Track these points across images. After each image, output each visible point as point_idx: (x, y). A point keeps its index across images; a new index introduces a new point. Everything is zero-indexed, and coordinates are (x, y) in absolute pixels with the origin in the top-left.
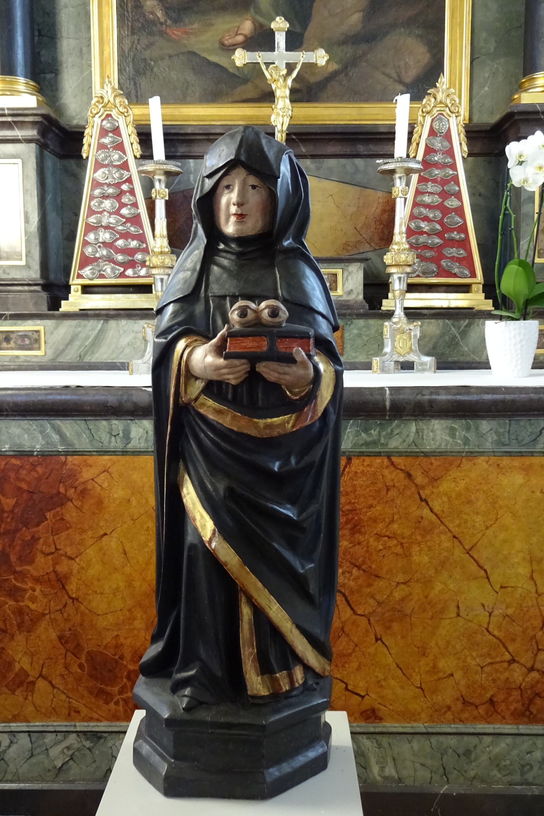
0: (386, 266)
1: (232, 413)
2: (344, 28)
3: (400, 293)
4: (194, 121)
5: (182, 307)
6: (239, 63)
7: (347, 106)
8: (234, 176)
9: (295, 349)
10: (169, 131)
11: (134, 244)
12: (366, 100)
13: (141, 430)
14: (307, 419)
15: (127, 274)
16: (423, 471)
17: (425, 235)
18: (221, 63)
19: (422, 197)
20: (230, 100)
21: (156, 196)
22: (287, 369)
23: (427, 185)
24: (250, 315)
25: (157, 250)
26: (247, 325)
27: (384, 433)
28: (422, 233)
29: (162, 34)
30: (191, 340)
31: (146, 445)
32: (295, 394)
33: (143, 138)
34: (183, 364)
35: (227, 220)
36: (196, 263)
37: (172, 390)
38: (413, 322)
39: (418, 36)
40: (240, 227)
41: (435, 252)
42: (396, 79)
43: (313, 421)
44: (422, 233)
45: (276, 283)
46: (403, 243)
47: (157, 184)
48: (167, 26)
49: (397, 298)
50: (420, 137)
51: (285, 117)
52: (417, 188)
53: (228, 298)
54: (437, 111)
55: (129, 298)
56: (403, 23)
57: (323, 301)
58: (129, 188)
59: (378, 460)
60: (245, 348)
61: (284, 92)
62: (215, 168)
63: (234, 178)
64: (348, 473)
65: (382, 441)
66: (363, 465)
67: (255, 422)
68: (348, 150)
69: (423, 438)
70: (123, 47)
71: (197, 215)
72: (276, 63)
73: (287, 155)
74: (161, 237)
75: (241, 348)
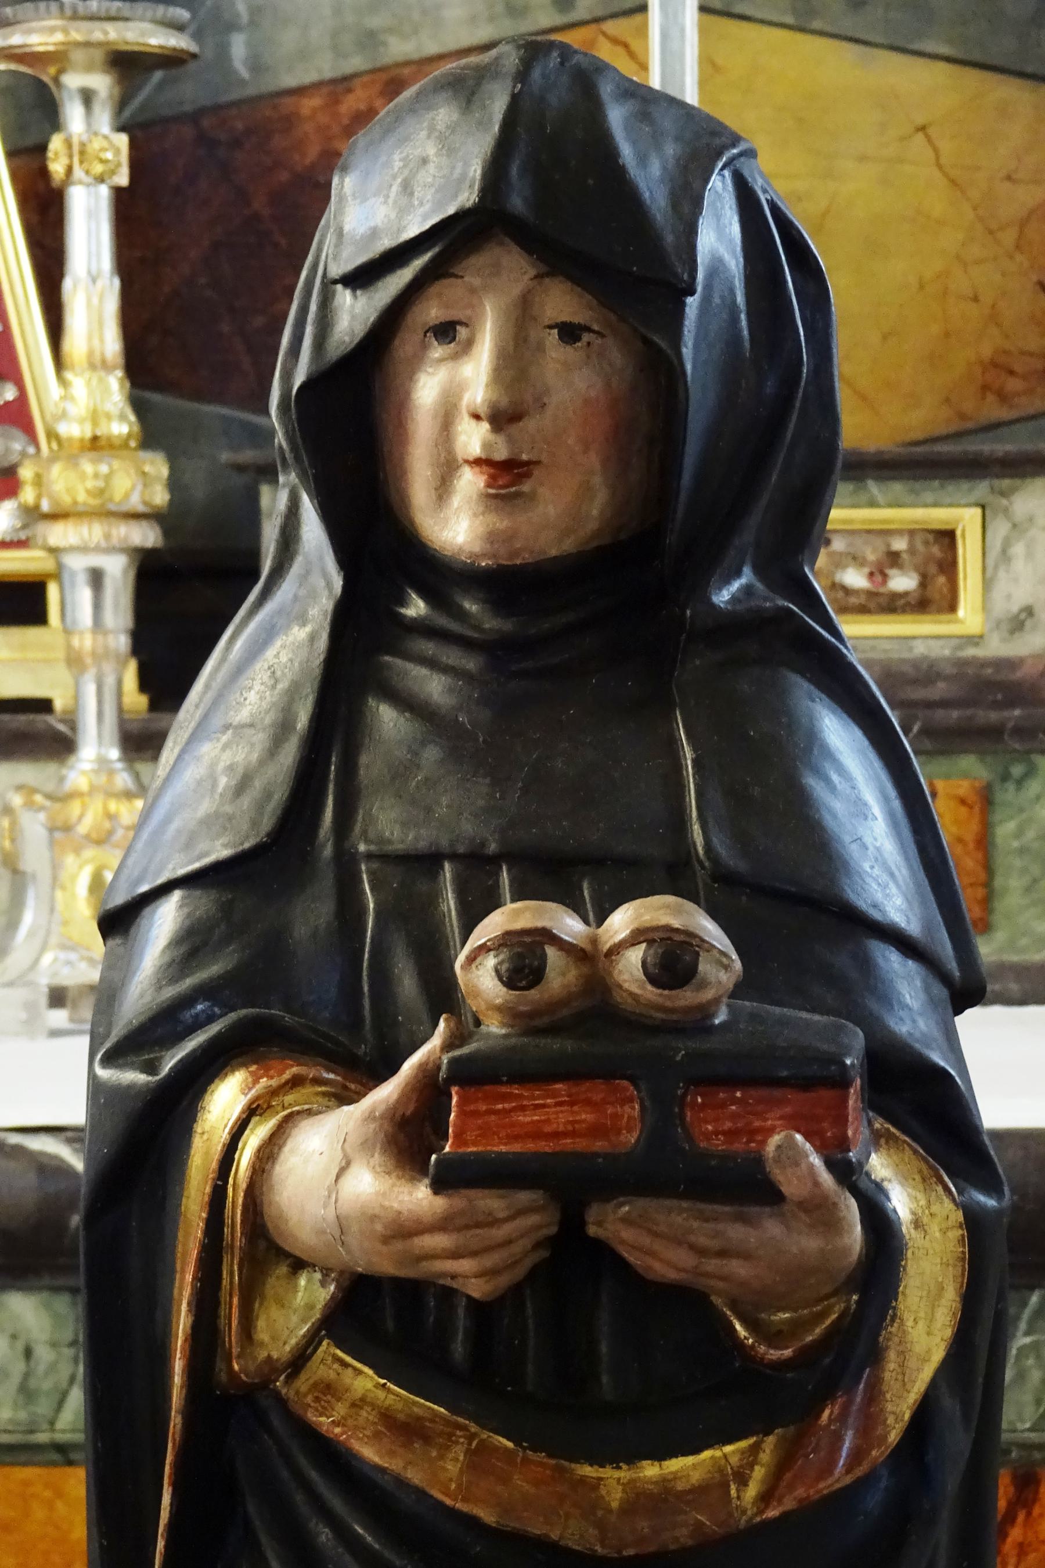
1: (471, 1437)
5: (226, 910)
8: (476, 281)
9: (775, 1140)
14: (832, 1462)
21: (69, 170)
22: (736, 1233)
25: (73, 430)
30: (274, 1082)
31: (22, 1415)
32: (774, 1337)
36: (292, 693)
37: (183, 1322)
40: (501, 523)
43: (860, 1471)
47: (74, 116)
53: (448, 869)
57: (903, 873)
60: (536, 1133)
62: (386, 243)
63: (473, 291)
67: (583, 1480)
71: (297, 459)
73: (726, 173)
75: (516, 1138)
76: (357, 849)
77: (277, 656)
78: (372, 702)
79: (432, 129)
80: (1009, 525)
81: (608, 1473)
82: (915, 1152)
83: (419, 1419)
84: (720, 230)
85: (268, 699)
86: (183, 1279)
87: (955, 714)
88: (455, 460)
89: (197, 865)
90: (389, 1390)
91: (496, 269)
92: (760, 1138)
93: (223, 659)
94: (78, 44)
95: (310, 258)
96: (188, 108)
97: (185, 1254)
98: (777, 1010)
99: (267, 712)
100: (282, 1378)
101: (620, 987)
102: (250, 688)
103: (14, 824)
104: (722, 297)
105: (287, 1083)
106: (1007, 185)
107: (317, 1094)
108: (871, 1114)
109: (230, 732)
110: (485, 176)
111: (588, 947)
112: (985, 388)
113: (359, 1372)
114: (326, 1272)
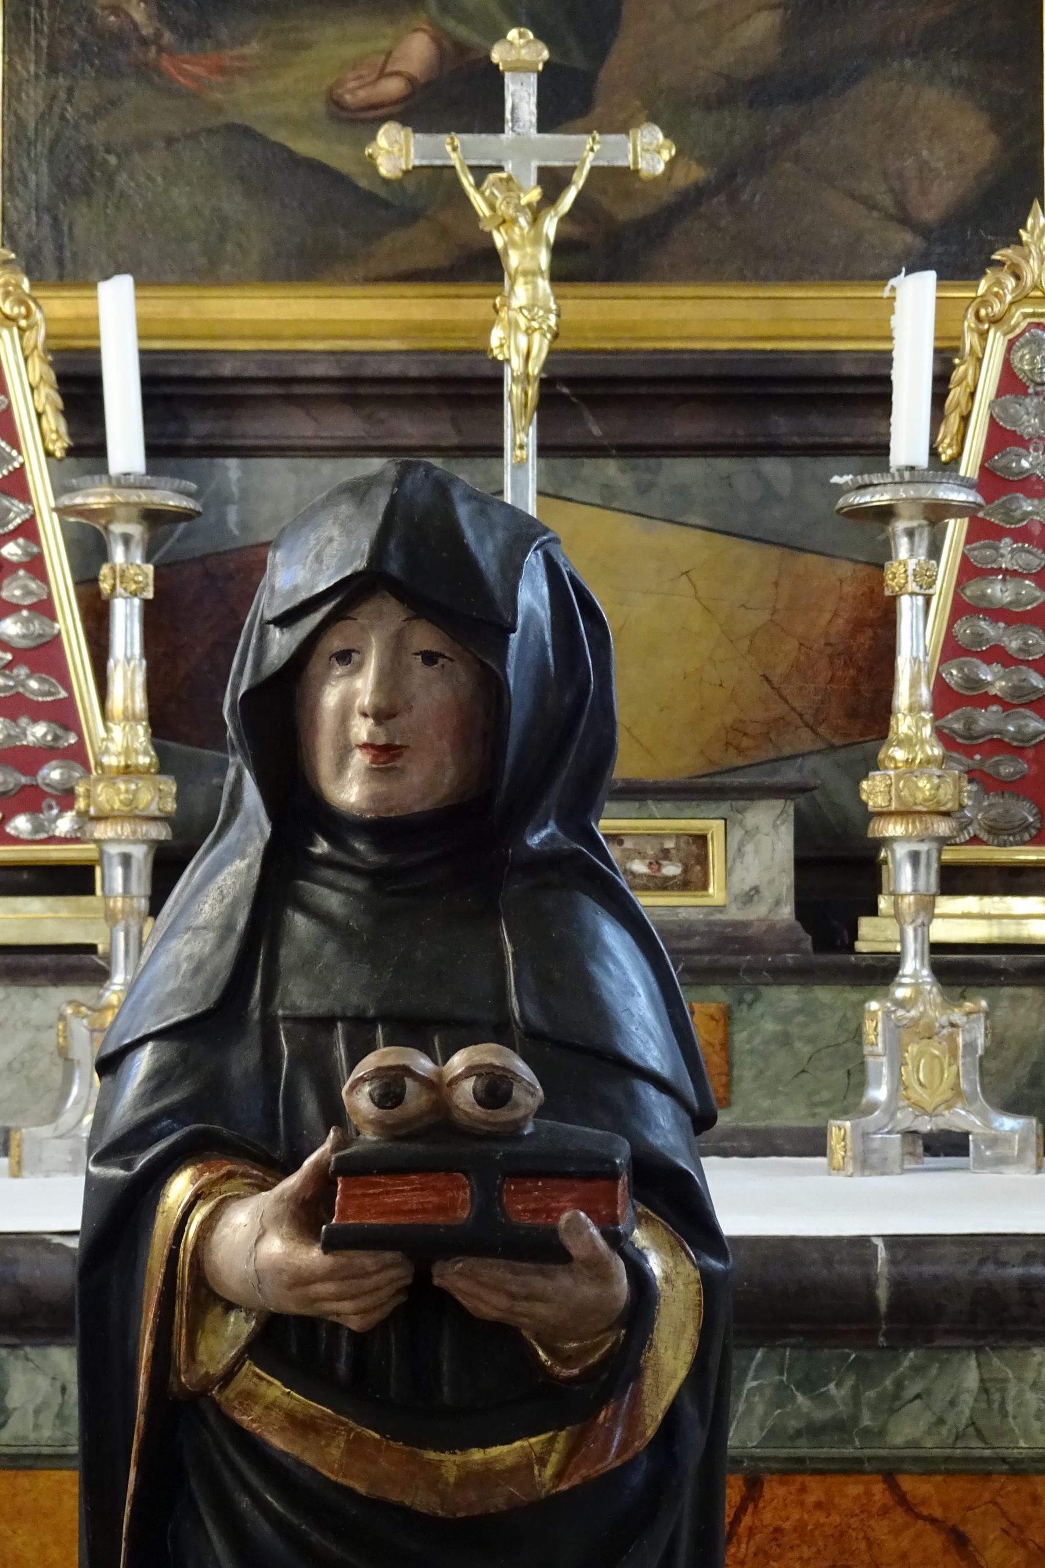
0: (870, 816)
2: (724, 57)
3: (916, 903)
4: (242, 338)
5: (184, 1056)
6: (386, 168)
7: (734, 294)
9: (566, 1216)
10: (162, 371)
11: (38, 732)
12: (796, 277)
13: (43, 1383)
15: (12, 832)
16: (1005, 1525)
17: (994, 708)
18: (334, 163)
19: (983, 584)
20: (361, 272)
22: (538, 1283)
23: (997, 549)
24: (415, 1098)
25: (111, 761)
26: (403, 1132)
27: (871, 1394)
28: (986, 700)
29: (144, 72)
30: (214, 1176)
31: (59, 1434)
32: (567, 1360)
33: (77, 390)
34: (185, 1257)
35: (344, 752)
36: (234, 905)
38: (963, 997)
39: (957, 83)
40: (382, 788)
41: (1028, 761)
42: (892, 211)
43: (626, 1457)
44: (986, 700)
45: (504, 972)
46: (922, 742)
47: (118, 554)
48: (161, 50)
49: (909, 919)
50: (972, 395)
51: (537, 336)
52: (964, 554)
54: (1026, 316)
55: (15, 911)
56: (908, 43)
58: (26, 553)
59: (854, 1489)
60: (397, 1211)
61: (534, 257)
62: (304, 595)
63: (362, 628)
64: (751, 1531)
65: (866, 1420)
66: (802, 1504)
67: (429, 1462)
68: (741, 432)
69: (1004, 1413)
70: (21, 112)
71: (241, 745)
72: (509, 166)
73: (539, 552)
74: (126, 718)
75: (382, 1214)
76: (277, 1015)
77: (225, 880)
78: (290, 912)
79: (336, 518)
80: (742, 832)
81: (446, 1456)
82: (666, 1229)
83: (313, 1417)
84: (535, 591)
85: (217, 910)
86: (147, 1316)
87: (707, 958)
88: (349, 745)
89: (164, 1024)
90: (292, 1397)
91: (380, 615)
92: (555, 1215)
93: (187, 884)
94: (121, 504)
95: (253, 608)
96: (198, 554)
97: (149, 1298)
98: (569, 1126)
99: (217, 918)
100: (217, 1388)
101: (457, 1107)
102: (205, 902)
103: (65, 1026)
104: (535, 637)
105: (222, 1176)
106: (742, 610)
107: (245, 1184)
108: (635, 1201)
109: (190, 932)
110: (372, 549)
111: (435, 1080)
112: (728, 744)
113: (270, 1383)
114: (249, 1311)
